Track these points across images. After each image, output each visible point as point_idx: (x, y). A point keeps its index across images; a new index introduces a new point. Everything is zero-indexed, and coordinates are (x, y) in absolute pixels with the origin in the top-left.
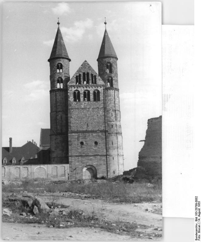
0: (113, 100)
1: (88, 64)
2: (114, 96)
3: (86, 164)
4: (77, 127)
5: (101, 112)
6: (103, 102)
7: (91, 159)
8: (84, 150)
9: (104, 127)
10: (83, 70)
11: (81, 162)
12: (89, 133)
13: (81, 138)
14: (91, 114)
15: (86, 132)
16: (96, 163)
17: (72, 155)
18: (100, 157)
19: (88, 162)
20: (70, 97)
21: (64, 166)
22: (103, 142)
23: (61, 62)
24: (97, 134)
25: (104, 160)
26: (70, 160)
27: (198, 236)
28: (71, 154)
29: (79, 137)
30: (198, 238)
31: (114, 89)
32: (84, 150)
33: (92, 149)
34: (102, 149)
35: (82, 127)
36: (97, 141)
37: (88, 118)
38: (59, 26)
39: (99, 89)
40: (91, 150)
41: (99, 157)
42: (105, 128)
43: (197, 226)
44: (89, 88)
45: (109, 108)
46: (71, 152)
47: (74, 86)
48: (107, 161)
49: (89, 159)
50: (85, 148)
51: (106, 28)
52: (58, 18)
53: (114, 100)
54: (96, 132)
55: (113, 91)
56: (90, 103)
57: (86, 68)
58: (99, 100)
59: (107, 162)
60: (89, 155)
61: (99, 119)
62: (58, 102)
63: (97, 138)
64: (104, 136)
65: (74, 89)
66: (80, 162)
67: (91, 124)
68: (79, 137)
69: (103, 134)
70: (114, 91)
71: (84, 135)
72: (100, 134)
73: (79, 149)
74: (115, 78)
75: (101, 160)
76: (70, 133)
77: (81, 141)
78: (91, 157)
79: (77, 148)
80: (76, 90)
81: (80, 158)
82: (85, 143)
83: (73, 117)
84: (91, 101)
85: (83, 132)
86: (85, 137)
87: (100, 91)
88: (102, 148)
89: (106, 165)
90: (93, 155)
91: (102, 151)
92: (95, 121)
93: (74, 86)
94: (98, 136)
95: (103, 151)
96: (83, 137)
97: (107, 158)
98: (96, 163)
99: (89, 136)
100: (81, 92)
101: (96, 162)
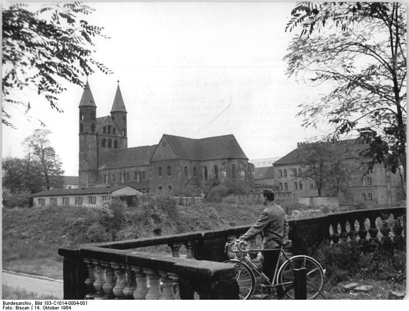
27: (10, 306)
30: (7, 306)
43: (27, 304)
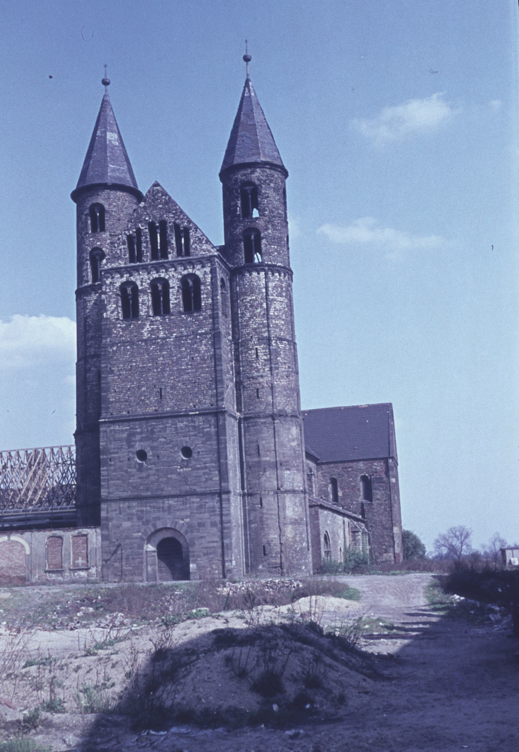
0: (261, 304)
1: (165, 194)
2: (264, 290)
3: (154, 525)
4: (126, 401)
5: (203, 348)
6: (209, 312)
7: (170, 507)
8: (148, 476)
9: (212, 396)
10: (148, 214)
11: (139, 518)
12: (165, 421)
13: (138, 437)
14: (171, 356)
15: (158, 417)
16: (188, 520)
17: (112, 495)
18: (198, 500)
19: (158, 518)
20: (108, 307)
21: (86, 535)
22: (209, 447)
23: (101, 201)
24: (188, 421)
25: (212, 510)
26: (103, 514)
28: (109, 493)
29: (132, 435)
31: (267, 268)
32: (148, 476)
33: (174, 472)
34: (205, 471)
35: (142, 401)
36: (188, 445)
37: (163, 370)
38: (106, 91)
39: (199, 272)
40: (169, 476)
41: (196, 499)
42: (217, 401)
44: (167, 271)
45: (248, 334)
46: (108, 488)
47: (118, 270)
48: (221, 511)
49: (163, 507)
50: (151, 472)
51: (248, 75)
52: (105, 66)
53: (264, 305)
54: (187, 416)
55: (262, 274)
56: (170, 320)
57: (157, 205)
58: (198, 308)
59: (221, 515)
60: (164, 493)
61: (196, 371)
62: (90, 326)
63: (190, 436)
64: (212, 427)
65: (119, 281)
66: (135, 519)
67: (172, 388)
68: (132, 435)
69: (209, 421)
70: (266, 274)
71: (149, 429)
72: (200, 421)
73: (133, 476)
74: (270, 231)
75: (203, 510)
76: (105, 422)
77: (138, 447)
78: (171, 502)
79: (127, 472)
80: (128, 283)
81: (134, 504)
82: (150, 454)
83: (115, 369)
84: (172, 315)
85: (145, 419)
86: (150, 436)
87: (201, 276)
88: (206, 468)
89: (219, 526)
90: (178, 492)
91: (207, 480)
92: (186, 377)
93: (121, 268)
94: (194, 427)
95: (211, 479)
96: (144, 435)
97: (221, 501)
98: (188, 520)
99: (165, 431)
100: (140, 288)
101: (187, 517)
